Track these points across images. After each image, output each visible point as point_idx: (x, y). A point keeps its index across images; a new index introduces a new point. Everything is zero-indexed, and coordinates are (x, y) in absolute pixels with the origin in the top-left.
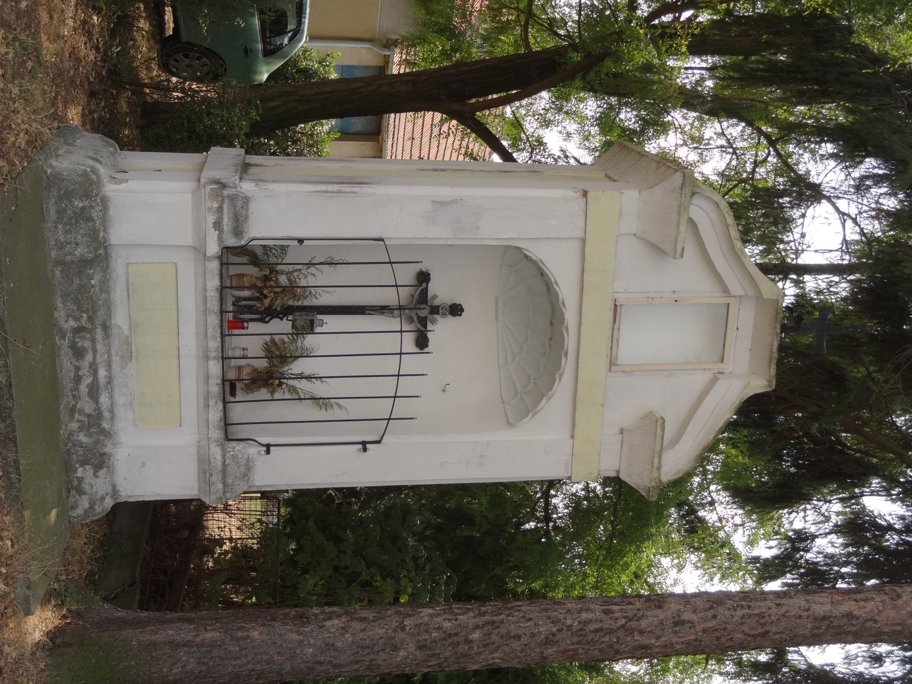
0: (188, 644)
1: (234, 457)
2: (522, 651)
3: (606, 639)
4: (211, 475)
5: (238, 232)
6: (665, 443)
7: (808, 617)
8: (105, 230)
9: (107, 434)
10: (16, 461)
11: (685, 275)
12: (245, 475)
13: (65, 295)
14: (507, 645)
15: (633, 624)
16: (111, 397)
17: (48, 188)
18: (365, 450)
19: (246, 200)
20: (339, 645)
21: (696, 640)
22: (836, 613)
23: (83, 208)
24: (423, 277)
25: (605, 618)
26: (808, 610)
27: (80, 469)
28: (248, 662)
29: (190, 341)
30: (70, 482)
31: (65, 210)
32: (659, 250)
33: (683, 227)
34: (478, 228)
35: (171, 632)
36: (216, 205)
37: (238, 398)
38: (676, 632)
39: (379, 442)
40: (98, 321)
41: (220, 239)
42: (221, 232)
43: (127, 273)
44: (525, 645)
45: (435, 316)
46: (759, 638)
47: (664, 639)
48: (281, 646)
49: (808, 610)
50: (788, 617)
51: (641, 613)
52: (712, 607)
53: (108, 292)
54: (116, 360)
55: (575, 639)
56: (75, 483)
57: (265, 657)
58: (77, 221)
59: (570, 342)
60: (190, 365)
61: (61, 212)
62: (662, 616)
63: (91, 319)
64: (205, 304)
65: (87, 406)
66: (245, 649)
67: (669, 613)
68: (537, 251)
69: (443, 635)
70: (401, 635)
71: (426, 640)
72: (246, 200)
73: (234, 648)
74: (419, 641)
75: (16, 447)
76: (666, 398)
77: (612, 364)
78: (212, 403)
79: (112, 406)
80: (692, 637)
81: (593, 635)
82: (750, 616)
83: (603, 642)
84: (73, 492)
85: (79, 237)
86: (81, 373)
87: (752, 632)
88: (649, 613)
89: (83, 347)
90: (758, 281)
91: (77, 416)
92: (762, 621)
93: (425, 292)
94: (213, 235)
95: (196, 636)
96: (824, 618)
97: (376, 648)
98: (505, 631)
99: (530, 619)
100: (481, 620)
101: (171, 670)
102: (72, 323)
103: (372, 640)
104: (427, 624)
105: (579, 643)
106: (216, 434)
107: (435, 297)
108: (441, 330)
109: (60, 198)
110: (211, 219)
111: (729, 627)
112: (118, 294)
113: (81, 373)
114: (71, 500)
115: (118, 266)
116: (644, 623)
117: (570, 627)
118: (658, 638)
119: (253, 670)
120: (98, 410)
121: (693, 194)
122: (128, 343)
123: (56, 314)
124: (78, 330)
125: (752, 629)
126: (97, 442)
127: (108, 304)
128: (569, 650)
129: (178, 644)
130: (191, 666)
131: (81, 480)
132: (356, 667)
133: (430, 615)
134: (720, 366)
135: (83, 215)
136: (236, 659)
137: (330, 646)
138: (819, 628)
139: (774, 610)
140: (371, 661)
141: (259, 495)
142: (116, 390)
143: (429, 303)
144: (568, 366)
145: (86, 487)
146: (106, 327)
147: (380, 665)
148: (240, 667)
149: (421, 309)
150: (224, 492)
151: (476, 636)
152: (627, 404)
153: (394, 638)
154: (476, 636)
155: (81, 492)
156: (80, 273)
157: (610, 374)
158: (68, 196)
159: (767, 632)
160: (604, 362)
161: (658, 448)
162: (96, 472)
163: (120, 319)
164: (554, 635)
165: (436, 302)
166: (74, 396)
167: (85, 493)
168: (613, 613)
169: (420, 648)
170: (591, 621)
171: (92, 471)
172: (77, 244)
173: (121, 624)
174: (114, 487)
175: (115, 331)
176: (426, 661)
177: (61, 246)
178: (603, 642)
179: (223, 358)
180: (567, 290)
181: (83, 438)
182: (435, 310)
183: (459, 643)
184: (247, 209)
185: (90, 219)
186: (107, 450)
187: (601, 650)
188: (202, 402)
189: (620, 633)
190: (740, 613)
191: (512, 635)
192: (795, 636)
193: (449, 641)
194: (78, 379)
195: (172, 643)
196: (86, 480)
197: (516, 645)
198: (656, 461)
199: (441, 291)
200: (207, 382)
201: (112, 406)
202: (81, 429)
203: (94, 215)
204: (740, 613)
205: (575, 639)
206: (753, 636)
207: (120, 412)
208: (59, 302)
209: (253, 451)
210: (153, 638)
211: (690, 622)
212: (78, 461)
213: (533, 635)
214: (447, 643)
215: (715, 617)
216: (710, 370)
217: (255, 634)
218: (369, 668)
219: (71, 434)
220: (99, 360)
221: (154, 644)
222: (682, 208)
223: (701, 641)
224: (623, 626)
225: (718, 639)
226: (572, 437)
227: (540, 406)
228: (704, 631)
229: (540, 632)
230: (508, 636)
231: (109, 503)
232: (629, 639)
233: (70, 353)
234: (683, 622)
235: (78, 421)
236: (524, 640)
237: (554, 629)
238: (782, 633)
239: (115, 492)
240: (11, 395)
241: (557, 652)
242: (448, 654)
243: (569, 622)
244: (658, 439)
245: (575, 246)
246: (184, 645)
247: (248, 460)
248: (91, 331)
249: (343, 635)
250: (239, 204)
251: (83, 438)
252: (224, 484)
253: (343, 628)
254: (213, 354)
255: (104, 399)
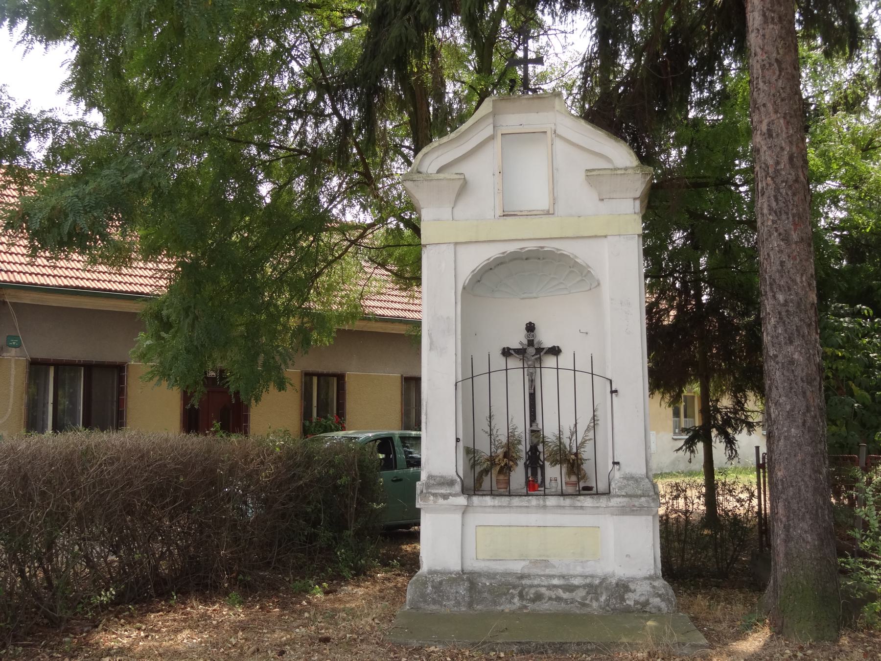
0: (787, 528)
1: (620, 488)
2: (795, 259)
3: (783, 191)
4: (634, 506)
5: (451, 483)
6: (611, 167)
7: (764, 29)
8: (451, 573)
9: (604, 580)
10: (578, 644)
11: (481, 170)
12: (637, 480)
13: (495, 603)
14: (789, 272)
15: (771, 170)
16: (575, 576)
17: (418, 609)
18: (616, 391)
19: (430, 477)
20: (788, 407)
21: (784, 118)
22: (760, 7)
23: (433, 587)
24: (506, 353)
25: (766, 194)
26: (758, 30)
27: (628, 602)
28: (803, 480)
29: (534, 518)
30: (638, 611)
31: (433, 599)
32: (464, 188)
33: (441, 176)
34: (448, 318)
35: (779, 541)
36: (432, 498)
37: (594, 485)
38: (778, 135)
39: (611, 381)
40: (517, 582)
41: (455, 495)
42: (451, 495)
43: (484, 560)
44: (789, 257)
45: (535, 342)
46: (783, 66)
47: (783, 145)
48: (789, 454)
49: (758, 30)
50: (764, 46)
51: (763, 165)
52: (758, 108)
53: (495, 574)
54: (548, 571)
55: (784, 217)
56: (639, 606)
57: (799, 466)
58: (441, 592)
59: (531, 246)
60: (550, 518)
61: (434, 602)
62: (765, 148)
63: (515, 587)
64: (504, 507)
65: (580, 594)
66: (791, 483)
67: (762, 143)
68: (465, 275)
69: (781, 324)
70: (780, 358)
71: (785, 338)
72: (430, 477)
73: (791, 492)
74: (786, 343)
75: (566, 643)
76: (573, 170)
77: (548, 213)
78: (579, 504)
79: (581, 576)
80: (782, 121)
81: (780, 203)
82: (763, 77)
83: (787, 194)
84: (648, 609)
85: (452, 591)
86: (554, 597)
87: (777, 73)
88: (763, 158)
89: (534, 594)
90: (480, 116)
91: (587, 602)
92: (767, 66)
93: (517, 351)
94: (452, 500)
95: (781, 522)
96: (764, 15)
97: (792, 378)
98: (777, 274)
99: (768, 254)
100: (770, 294)
101: (808, 542)
102: (516, 600)
103: (784, 381)
104: (772, 337)
105: (787, 214)
106: (603, 502)
107: (521, 343)
108: (547, 339)
109: (425, 601)
110: (441, 501)
111: (773, 91)
112: (499, 567)
113: (554, 597)
114: (653, 610)
115: (474, 564)
116: (771, 162)
117: (774, 222)
118: (782, 149)
119: (810, 476)
120: (584, 586)
121: (420, 173)
122: (535, 562)
123: (507, 611)
124: (521, 596)
125: (774, 73)
126: (607, 589)
127: (506, 574)
128: (794, 221)
129: (787, 536)
130: (806, 527)
131: (637, 602)
132: (808, 393)
133: (767, 334)
134: (549, 133)
135: (438, 587)
136: (800, 490)
137: (790, 415)
138: (773, 18)
139: (759, 58)
140: (803, 381)
141: (761, 471)
142: (571, 572)
143: (525, 347)
144: (550, 246)
145: (643, 599)
146: (522, 577)
147: (807, 373)
148: (807, 487)
149: (532, 353)
150: (649, 496)
151: (781, 297)
152: (580, 196)
153: (783, 364)
154: (781, 297)
155: (646, 603)
156: (480, 592)
157: (556, 213)
158: (423, 596)
159: (777, 60)
160: (546, 219)
161: (609, 172)
162: (630, 591)
163: (517, 567)
164: (780, 234)
165: (525, 342)
166: (571, 603)
167: (648, 600)
168: (763, 188)
169: (791, 342)
170: (769, 206)
171: (630, 594)
172: (457, 592)
173: (775, 581)
174: (646, 578)
175: (526, 571)
176: (803, 336)
177: (458, 604)
178: (787, 194)
179: (545, 495)
180: (493, 252)
181: (603, 598)
182: (531, 343)
183: (787, 311)
184: (437, 477)
185: (441, 583)
186: (614, 581)
187: (794, 194)
188: (576, 511)
189: (778, 180)
190: (761, 85)
191: (780, 268)
192: (780, 37)
193: (785, 318)
194: (559, 599)
195: (787, 540)
196: (637, 598)
197: (789, 265)
198: (619, 172)
199: (517, 339)
200: (564, 507)
201: (581, 576)
202: (597, 600)
203: (439, 580)
204: (761, 85)
205: (784, 217)
206: (780, 71)
207: (588, 571)
208: (499, 608)
209: (617, 475)
210: (781, 555)
211: (768, 125)
212: (621, 603)
213: (781, 251)
214: (787, 320)
215: (764, 105)
216: (552, 140)
217: (779, 474)
218: (810, 383)
219: (600, 607)
220: (545, 583)
221: (786, 554)
222: (428, 179)
223: (785, 114)
224: (772, 179)
225: (782, 100)
226: (606, 236)
227: (582, 263)
228: (776, 112)
229: (778, 245)
230: (781, 272)
231: (660, 583)
232: (783, 173)
233: (538, 603)
234: (768, 130)
235: (591, 601)
236: (784, 258)
237: (776, 234)
238: (777, 48)
239: (651, 578)
240: (527, 643)
241: (795, 230)
242: (796, 319)
243: (770, 223)
244: (601, 172)
245: (461, 249)
246: (788, 531)
247: (624, 478)
248: (523, 587)
249: (780, 404)
250: (432, 482)
251: (603, 598)
252: (641, 496)
253: (776, 405)
254: (541, 502)
255: (576, 582)
